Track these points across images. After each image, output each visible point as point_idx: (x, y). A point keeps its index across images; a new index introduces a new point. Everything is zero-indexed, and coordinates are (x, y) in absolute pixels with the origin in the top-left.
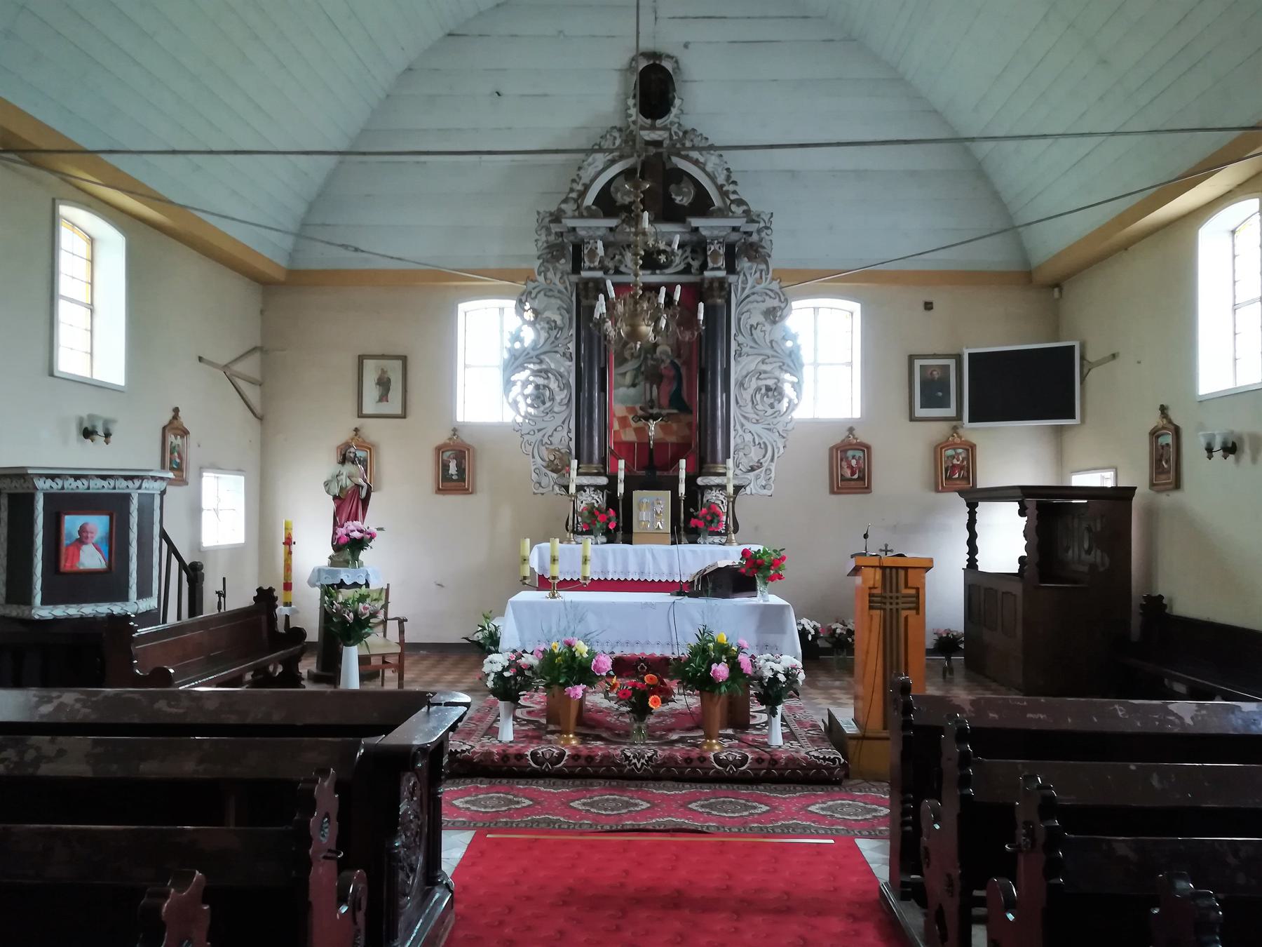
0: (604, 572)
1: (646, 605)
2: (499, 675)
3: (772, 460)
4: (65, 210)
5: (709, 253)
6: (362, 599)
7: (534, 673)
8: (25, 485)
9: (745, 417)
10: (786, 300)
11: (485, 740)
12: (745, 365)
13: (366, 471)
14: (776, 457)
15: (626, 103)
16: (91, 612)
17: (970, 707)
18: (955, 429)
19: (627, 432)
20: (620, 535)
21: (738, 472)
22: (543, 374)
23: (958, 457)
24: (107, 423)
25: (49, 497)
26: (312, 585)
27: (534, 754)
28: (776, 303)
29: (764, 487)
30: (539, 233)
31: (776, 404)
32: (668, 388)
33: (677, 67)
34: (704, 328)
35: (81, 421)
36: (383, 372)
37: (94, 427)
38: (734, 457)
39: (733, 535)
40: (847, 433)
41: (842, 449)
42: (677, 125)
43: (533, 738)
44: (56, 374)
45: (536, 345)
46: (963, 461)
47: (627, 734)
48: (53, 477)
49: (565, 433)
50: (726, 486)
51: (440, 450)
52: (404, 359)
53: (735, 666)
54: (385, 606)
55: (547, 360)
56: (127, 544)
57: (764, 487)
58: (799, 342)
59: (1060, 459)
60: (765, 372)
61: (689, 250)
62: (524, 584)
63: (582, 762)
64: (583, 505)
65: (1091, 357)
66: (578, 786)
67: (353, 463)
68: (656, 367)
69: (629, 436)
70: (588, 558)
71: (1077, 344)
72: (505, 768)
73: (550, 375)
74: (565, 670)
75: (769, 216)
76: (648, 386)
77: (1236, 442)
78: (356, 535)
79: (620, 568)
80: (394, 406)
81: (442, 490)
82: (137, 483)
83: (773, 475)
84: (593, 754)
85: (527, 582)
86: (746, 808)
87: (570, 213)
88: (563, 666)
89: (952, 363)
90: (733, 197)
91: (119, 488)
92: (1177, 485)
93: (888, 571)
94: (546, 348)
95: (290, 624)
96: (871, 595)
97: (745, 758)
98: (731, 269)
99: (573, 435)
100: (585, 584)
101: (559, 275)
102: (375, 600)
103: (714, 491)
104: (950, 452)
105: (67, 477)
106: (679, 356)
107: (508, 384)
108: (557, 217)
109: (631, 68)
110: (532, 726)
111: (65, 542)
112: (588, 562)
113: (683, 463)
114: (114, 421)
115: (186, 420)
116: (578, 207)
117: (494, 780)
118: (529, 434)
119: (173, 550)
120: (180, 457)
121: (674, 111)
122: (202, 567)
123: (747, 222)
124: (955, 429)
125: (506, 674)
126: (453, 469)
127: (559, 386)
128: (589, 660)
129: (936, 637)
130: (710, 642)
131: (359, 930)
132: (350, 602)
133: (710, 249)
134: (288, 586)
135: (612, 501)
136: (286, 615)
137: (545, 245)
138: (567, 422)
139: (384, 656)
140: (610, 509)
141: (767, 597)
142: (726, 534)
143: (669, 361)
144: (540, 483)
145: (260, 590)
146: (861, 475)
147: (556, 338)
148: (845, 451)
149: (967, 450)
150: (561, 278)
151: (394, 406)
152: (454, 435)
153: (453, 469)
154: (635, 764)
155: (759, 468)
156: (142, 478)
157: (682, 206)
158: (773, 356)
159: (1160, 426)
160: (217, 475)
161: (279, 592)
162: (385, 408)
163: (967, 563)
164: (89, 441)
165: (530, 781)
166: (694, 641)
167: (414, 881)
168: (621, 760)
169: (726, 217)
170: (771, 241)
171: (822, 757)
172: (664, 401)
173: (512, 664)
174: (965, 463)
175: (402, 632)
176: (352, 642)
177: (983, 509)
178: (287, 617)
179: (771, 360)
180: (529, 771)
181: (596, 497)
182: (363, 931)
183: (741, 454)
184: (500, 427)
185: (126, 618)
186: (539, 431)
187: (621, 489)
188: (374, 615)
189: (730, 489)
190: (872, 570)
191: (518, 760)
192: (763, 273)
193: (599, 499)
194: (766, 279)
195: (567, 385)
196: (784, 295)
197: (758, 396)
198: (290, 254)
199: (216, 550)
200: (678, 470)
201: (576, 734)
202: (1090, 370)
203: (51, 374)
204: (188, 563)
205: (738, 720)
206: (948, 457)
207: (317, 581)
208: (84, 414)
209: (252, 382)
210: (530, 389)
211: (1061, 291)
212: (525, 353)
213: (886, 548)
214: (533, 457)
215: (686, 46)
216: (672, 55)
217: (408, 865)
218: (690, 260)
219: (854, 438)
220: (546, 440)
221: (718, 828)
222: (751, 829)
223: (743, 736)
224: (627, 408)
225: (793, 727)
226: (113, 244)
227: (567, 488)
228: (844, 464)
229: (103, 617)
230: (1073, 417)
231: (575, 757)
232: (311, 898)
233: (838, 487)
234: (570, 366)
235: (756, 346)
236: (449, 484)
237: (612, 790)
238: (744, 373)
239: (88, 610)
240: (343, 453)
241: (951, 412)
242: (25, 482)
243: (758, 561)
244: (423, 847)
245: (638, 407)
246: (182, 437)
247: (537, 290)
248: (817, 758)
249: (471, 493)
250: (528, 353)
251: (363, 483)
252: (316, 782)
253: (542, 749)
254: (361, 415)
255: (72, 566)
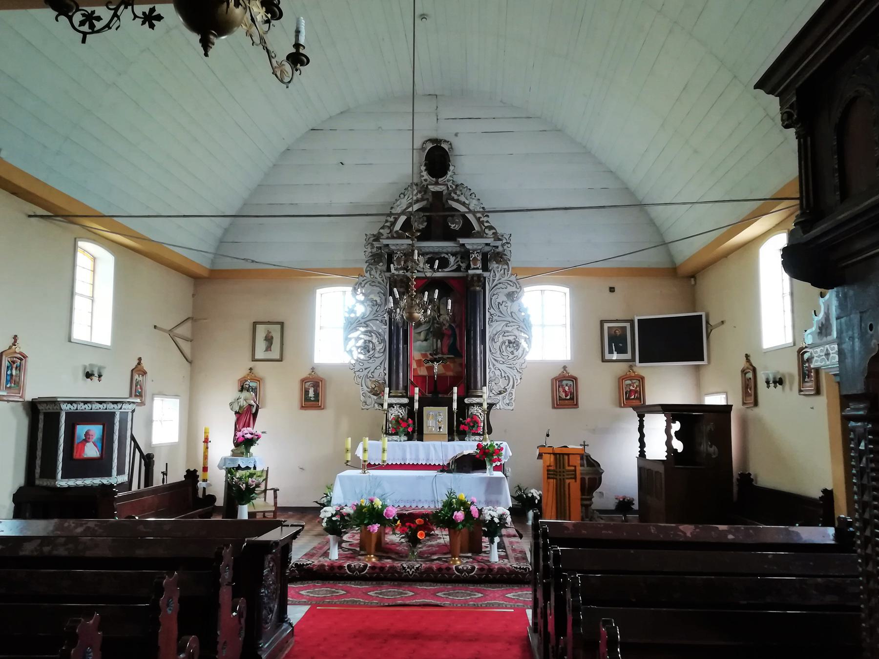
0: (404, 459)
1: (420, 478)
2: (330, 519)
3: (513, 387)
4: (81, 244)
5: (471, 259)
6: (251, 476)
7: (350, 518)
8: (55, 408)
9: (495, 360)
10: (520, 287)
11: (321, 559)
12: (495, 327)
13: (256, 395)
14: (515, 385)
15: (420, 169)
16: (90, 483)
17: (573, 528)
18: (631, 367)
19: (422, 370)
20: (415, 435)
21: (491, 395)
22: (368, 334)
23: (634, 385)
24: (100, 368)
25: (68, 414)
26: (221, 468)
27: (349, 566)
28: (514, 289)
29: (508, 404)
30: (366, 247)
31: (515, 351)
32: (448, 341)
33: (451, 148)
34: (451, 314)
35: (85, 368)
36: (269, 332)
37: (93, 371)
38: (489, 386)
39: (487, 435)
40: (562, 370)
41: (559, 380)
42: (452, 181)
43: (350, 558)
44: (72, 341)
45: (364, 316)
46: (636, 388)
47: (407, 556)
48: (71, 403)
49: (382, 370)
50: (482, 404)
51: (303, 381)
52: (282, 324)
53: (468, 513)
54: (266, 480)
55: (371, 325)
56: (112, 442)
57: (508, 404)
58: (529, 312)
59: (698, 385)
60: (508, 332)
61: (459, 257)
62: (348, 465)
63: (377, 570)
64: (392, 417)
65: (712, 322)
66: (374, 585)
67: (248, 391)
68: (440, 329)
69: (423, 372)
70: (385, 449)
71: (703, 314)
72: (332, 575)
73: (373, 334)
74: (368, 516)
75: (509, 236)
76: (435, 340)
77: (782, 377)
78: (249, 436)
79: (414, 457)
80: (275, 354)
81: (304, 407)
82: (120, 405)
83: (513, 397)
84: (384, 566)
85: (348, 464)
86: (470, 595)
87: (385, 235)
88: (367, 514)
89: (628, 325)
90: (486, 224)
91: (109, 409)
92: (756, 403)
93: (558, 456)
94: (371, 317)
95: (206, 492)
96: (548, 470)
97: (473, 568)
98: (485, 268)
99: (387, 372)
100: (383, 465)
101: (379, 272)
102: (259, 476)
103: (475, 407)
104: (629, 382)
105: (80, 402)
106: (454, 322)
107: (347, 340)
108: (377, 238)
109: (423, 149)
110: (351, 552)
111: (77, 441)
112: (385, 452)
113: (455, 389)
114: (104, 368)
115: (145, 365)
116: (390, 232)
117: (325, 582)
118: (359, 371)
119: (137, 446)
120: (141, 388)
121: (450, 173)
122: (153, 456)
123: (494, 240)
124: (631, 367)
125: (334, 519)
126: (311, 394)
127: (378, 341)
128: (382, 510)
129: (617, 501)
130: (454, 498)
131: (242, 628)
132: (244, 477)
133: (472, 257)
134: (205, 469)
135: (411, 413)
136: (204, 487)
137: (370, 254)
138: (383, 363)
139: (264, 512)
140: (410, 419)
141: (491, 473)
142: (483, 435)
143: (448, 325)
144: (365, 402)
145: (188, 471)
146: (572, 396)
147: (376, 311)
148: (561, 381)
149: (639, 381)
150: (380, 275)
151: (275, 354)
152: (313, 372)
153: (311, 394)
154: (408, 572)
155: (504, 392)
156: (122, 403)
157: (455, 230)
158: (513, 322)
159: (745, 368)
160: (162, 399)
161: (200, 473)
162: (269, 355)
163: (639, 453)
164: (89, 380)
165: (346, 582)
166: (445, 499)
167: (272, 617)
168: (400, 569)
169: (482, 237)
170: (510, 251)
171: (519, 567)
172: (445, 350)
173: (338, 513)
174: (638, 389)
175: (275, 497)
176: (244, 502)
177: (649, 418)
178: (204, 488)
179: (511, 324)
180: (346, 576)
181: (401, 411)
182: (244, 629)
183: (493, 383)
184: (343, 366)
185: (112, 486)
186: (366, 369)
187: (416, 406)
188: (258, 486)
189: (485, 406)
190: (549, 455)
191: (340, 570)
192: (506, 271)
193: (402, 413)
194: (508, 274)
195: (383, 341)
196: (519, 284)
197: (504, 347)
198: (212, 260)
199: (160, 446)
200: (452, 393)
201: (376, 556)
202: (711, 330)
203: (70, 341)
204: (145, 454)
205: (475, 548)
206: (627, 385)
207: (224, 466)
208: (87, 364)
209: (186, 340)
210: (360, 343)
211: (695, 280)
212: (358, 320)
213: (584, 443)
214: (362, 386)
215: (456, 135)
216: (447, 140)
217: (269, 607)
218: (460, 263)
219: (567, 373)
220: (370, 375)
221: (450, 604)
222: (469, 605)
223: (477, 557)
224: (422, 354)
225: (508, 553)
226: (107, 260)
227: (382, 405)
228: (561, 389)
229: (96, 486)
230: (703, 360)
231: (373, 568)
232: (220, 602)
233: (557, 405)
234: (385, 329)
235: (502, 315)
236: (308, 403)
237: (394, 586)
238: (495, 332)
239: (88, 482)
240: (242, 385)
241: (628, 356)
242: (55, 406)
243: (486, 450)
244: (277, 600)
245: (428, 353)
246: (143, 376)
247: (365, 282)
248: (516, 568)
249: (323, 409)
250: (359, 321)
251: (254, 404)
252: (223, 549)
253: (354, 564)
254: (254, 360)
255: (80, 455)
